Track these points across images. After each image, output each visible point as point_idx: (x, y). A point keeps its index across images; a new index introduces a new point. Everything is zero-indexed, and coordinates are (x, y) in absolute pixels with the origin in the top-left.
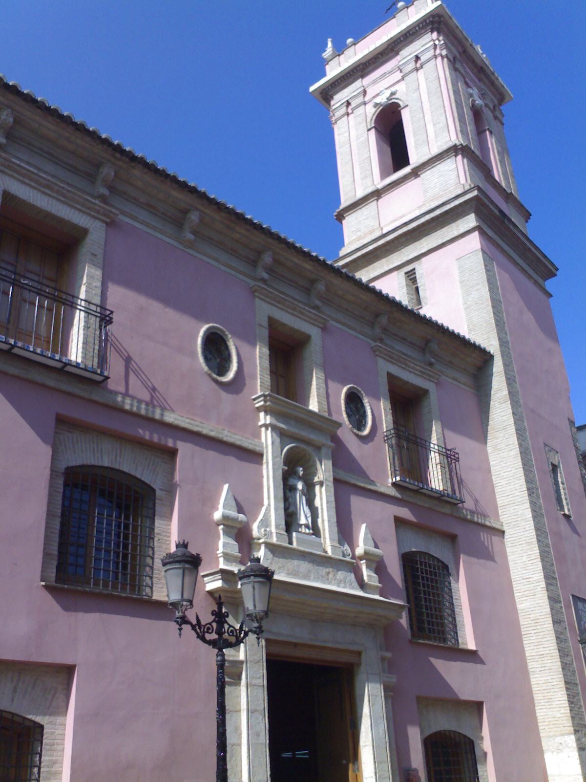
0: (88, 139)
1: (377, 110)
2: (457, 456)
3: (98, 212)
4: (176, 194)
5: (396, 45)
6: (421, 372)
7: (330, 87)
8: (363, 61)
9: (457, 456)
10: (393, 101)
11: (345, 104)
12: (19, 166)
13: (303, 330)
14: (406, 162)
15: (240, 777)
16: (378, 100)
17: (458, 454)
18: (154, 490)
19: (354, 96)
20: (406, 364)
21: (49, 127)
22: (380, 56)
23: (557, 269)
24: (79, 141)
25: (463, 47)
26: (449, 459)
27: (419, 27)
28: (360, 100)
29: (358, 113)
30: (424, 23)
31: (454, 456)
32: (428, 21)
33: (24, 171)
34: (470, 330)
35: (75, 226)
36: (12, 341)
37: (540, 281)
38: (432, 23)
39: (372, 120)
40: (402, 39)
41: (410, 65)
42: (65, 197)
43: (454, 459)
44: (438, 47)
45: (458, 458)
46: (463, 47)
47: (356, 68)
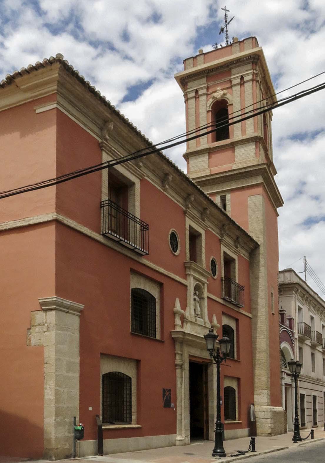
0: (139, 139)
1: (214, 100)
2: (147, 226)
3: (138, 174)
4: (165, 167)
5: (230, 64)
6: (234, 251)
7: (187, 77)
8: (210, 68)
9: (147, 226)
10: (224, 98)
11: (195, 91)
12: (114, 151)
13: (199, 231)
14: (227, 137)
15: (128, 378)
16: (215, 95)
17: (148, 225)
18: (155, 299)
19: (201, 88)
20: (229, 247)
21: (125, 131)
22: (220, 68)
23: (283, 203)
24: (135, 139)
25: (264, 74)
26: (142, 227)
27: (246, 58)
28: (205, 91)
29: (202, 99)
30: (250, 57)
31: (145, 226)
32: (252, 57)
33: (116, 154)
34: (231, 216)
35: (130, 181)
36: (121, 238)
37: (275, 207)
38: (254, 58)
39: (210, 105)
40: (235, 62)
41: (237, 80)
42: (128, 167)
43: (145, 228)
44: (255, 74)
45: (148, 228)
46: (264, 74)
47: (204, 71)
